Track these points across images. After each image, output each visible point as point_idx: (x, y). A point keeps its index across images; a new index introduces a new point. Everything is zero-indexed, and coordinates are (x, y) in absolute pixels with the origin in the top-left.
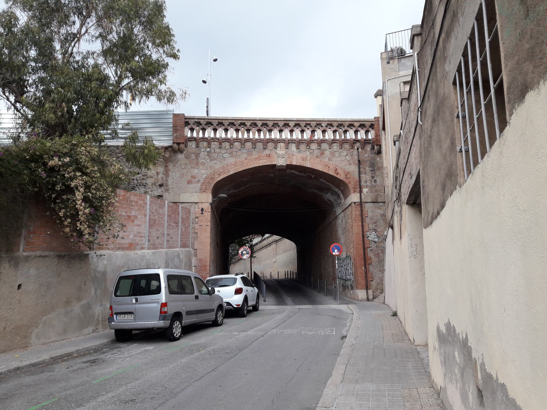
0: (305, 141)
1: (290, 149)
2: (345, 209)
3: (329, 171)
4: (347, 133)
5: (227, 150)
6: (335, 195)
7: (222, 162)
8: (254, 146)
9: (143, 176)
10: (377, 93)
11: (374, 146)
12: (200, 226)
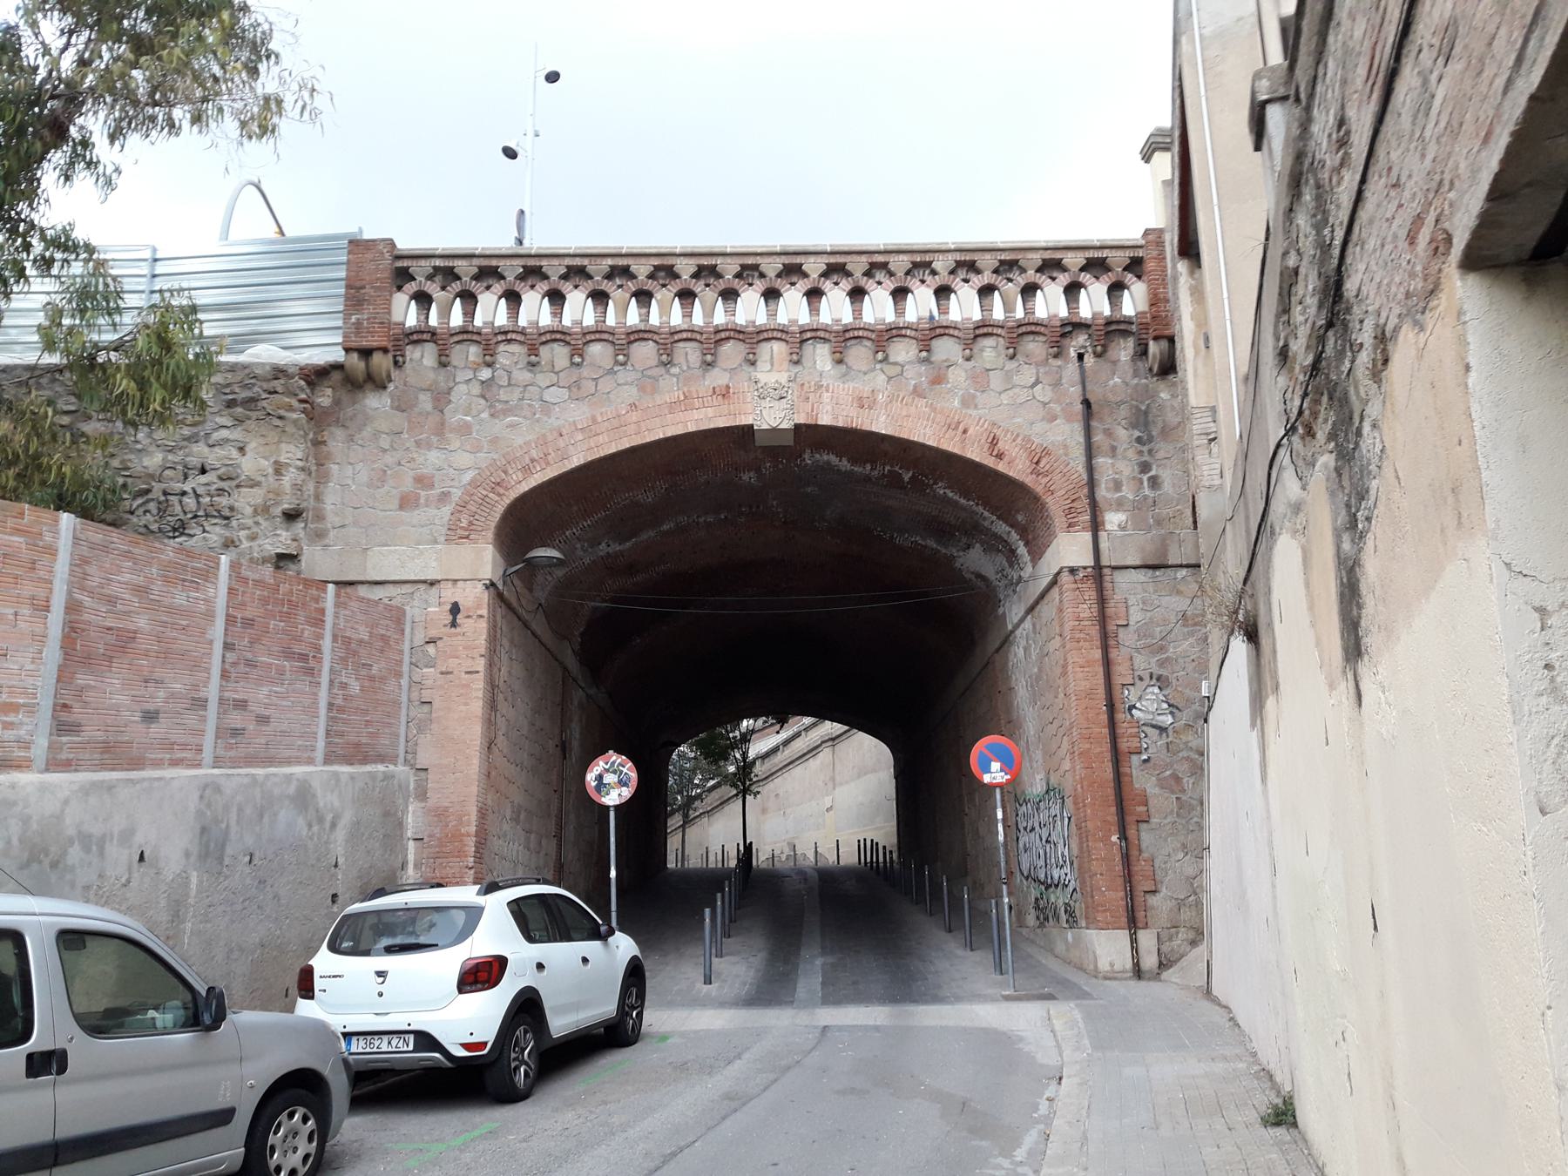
0: (866, 334)
1: (806, 361)
2: (1037, 602)
5: (557, 373)
6: (1000, 551)
9: (221, 478)
11: (1147, 345)
12: (442, 673)
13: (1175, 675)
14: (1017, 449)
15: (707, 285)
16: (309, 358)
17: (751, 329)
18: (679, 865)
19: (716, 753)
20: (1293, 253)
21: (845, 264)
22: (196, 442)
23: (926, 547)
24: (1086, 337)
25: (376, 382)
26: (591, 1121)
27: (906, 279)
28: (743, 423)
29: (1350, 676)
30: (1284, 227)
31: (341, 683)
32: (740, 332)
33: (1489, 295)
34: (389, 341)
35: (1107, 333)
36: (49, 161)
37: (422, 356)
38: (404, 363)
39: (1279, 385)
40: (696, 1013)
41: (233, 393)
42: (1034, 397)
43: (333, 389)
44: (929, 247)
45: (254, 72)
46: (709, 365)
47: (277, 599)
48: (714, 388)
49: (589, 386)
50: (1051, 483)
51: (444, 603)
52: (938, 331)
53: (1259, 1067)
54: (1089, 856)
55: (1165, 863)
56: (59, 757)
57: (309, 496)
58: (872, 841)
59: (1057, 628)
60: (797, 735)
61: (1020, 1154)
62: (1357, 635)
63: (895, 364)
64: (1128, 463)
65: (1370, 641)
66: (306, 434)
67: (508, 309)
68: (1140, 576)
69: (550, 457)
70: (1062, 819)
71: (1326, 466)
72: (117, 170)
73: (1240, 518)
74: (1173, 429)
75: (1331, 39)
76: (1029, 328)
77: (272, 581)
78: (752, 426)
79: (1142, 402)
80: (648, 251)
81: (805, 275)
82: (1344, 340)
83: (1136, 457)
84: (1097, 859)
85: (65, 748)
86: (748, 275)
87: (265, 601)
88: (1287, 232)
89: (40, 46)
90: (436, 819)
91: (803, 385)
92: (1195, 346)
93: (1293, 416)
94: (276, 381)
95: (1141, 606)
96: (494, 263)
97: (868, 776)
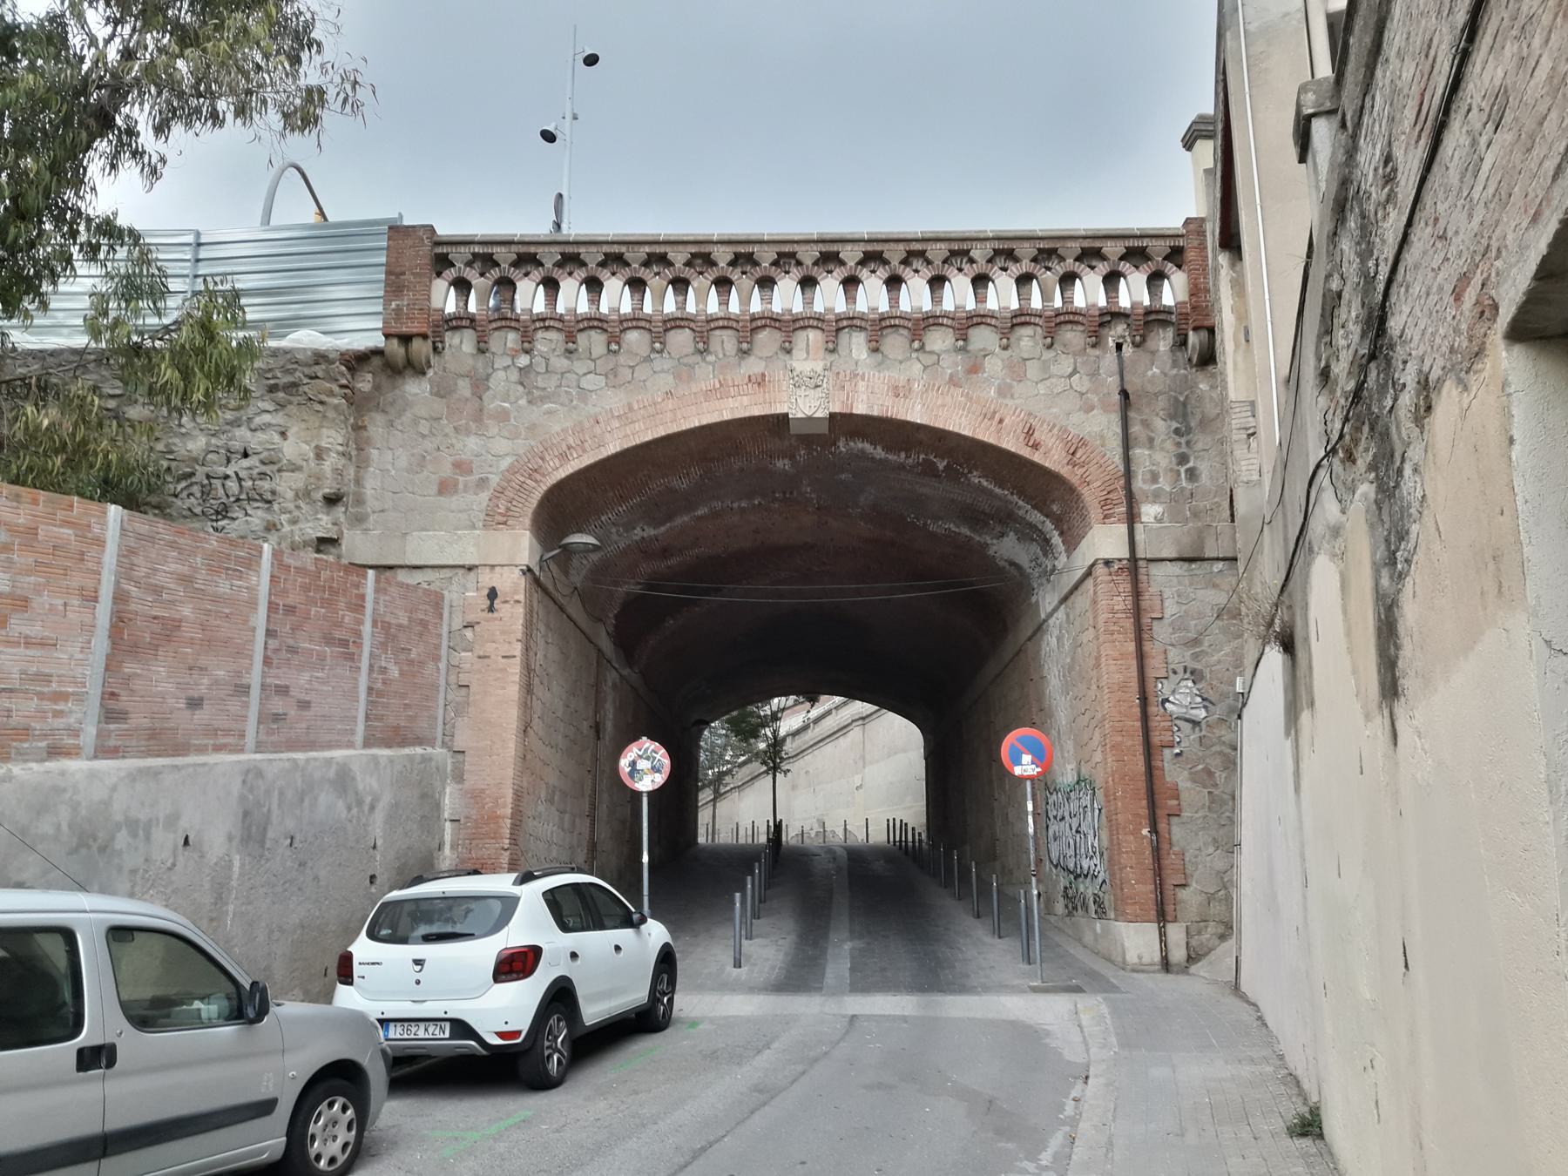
0: (902, 322)
2: (1071, 592)
3: (999, 438)
4: (1073, 284)
6: (1035, 540)
7: (575, 408)
8: (701, 346)
9: (263, 463)
10: (1194, 128)
11: (1186, 335)
12: (480, 657)
16: (348, 344)
17: (787, 317)
18: (710, 841)
19: (746, 731)
20: (1336, 276)
21: (883, 252)
22: (239, 426)
23: (959, 534)
24: (1125, 326)
26: (622, 1111)
27: (943, 267)
28: (778, 411)
29: (1386, 712)
30: (1327, 251)
31: (381, 667)
32: (776, 320)
33: (1534, 367)
34: (429, 327)
35: (1146, 323)
36: (96, 150)
37: (461, 342)
38: (443, 349)
39: (1319, 406)
40: (726, 998)
41: (275, 377)
42: (1071, 387)
43: (373, 374)
44: (967, 235)
45: (295, 60)
46: (745, 353)
47: (319, 586)
48: (749, 377)
49: (626, 374)
52: (975, 320)
53: (1286, 1071)
54: (1120, 849)
55: (1196, 857)
56: (106, 744)
57: (350, 481)
58: (901, 821)
59: (1091, 619)
60: (828, 713)
61: (1046, 1158)
62: (1394, 675)
63: (932, 352)
64: (1165, 454)
65: (1408, 683)
66: (347, 419)
68: (1176, 569)
69: (586, 445)
70: (1093, 810)
71: (1366, 496)
72: (163, 160)
73: (1279, 522)
75: (1379, 73)
77: (314, 568)
78: (787, 414)
79: (1181, 393)
80: (685, 238)
81: (842, 263)
82: (1387, 375)
84: (1127, 852)
85: (113, 734)
86: (784, 263)
87: (306, 588)
88: (1331, 255)
89: (85, 37)
90: (473, 801)
91: (838, 373)
93: (1335, 436)
94: (317, 367)
96: (532, 249)
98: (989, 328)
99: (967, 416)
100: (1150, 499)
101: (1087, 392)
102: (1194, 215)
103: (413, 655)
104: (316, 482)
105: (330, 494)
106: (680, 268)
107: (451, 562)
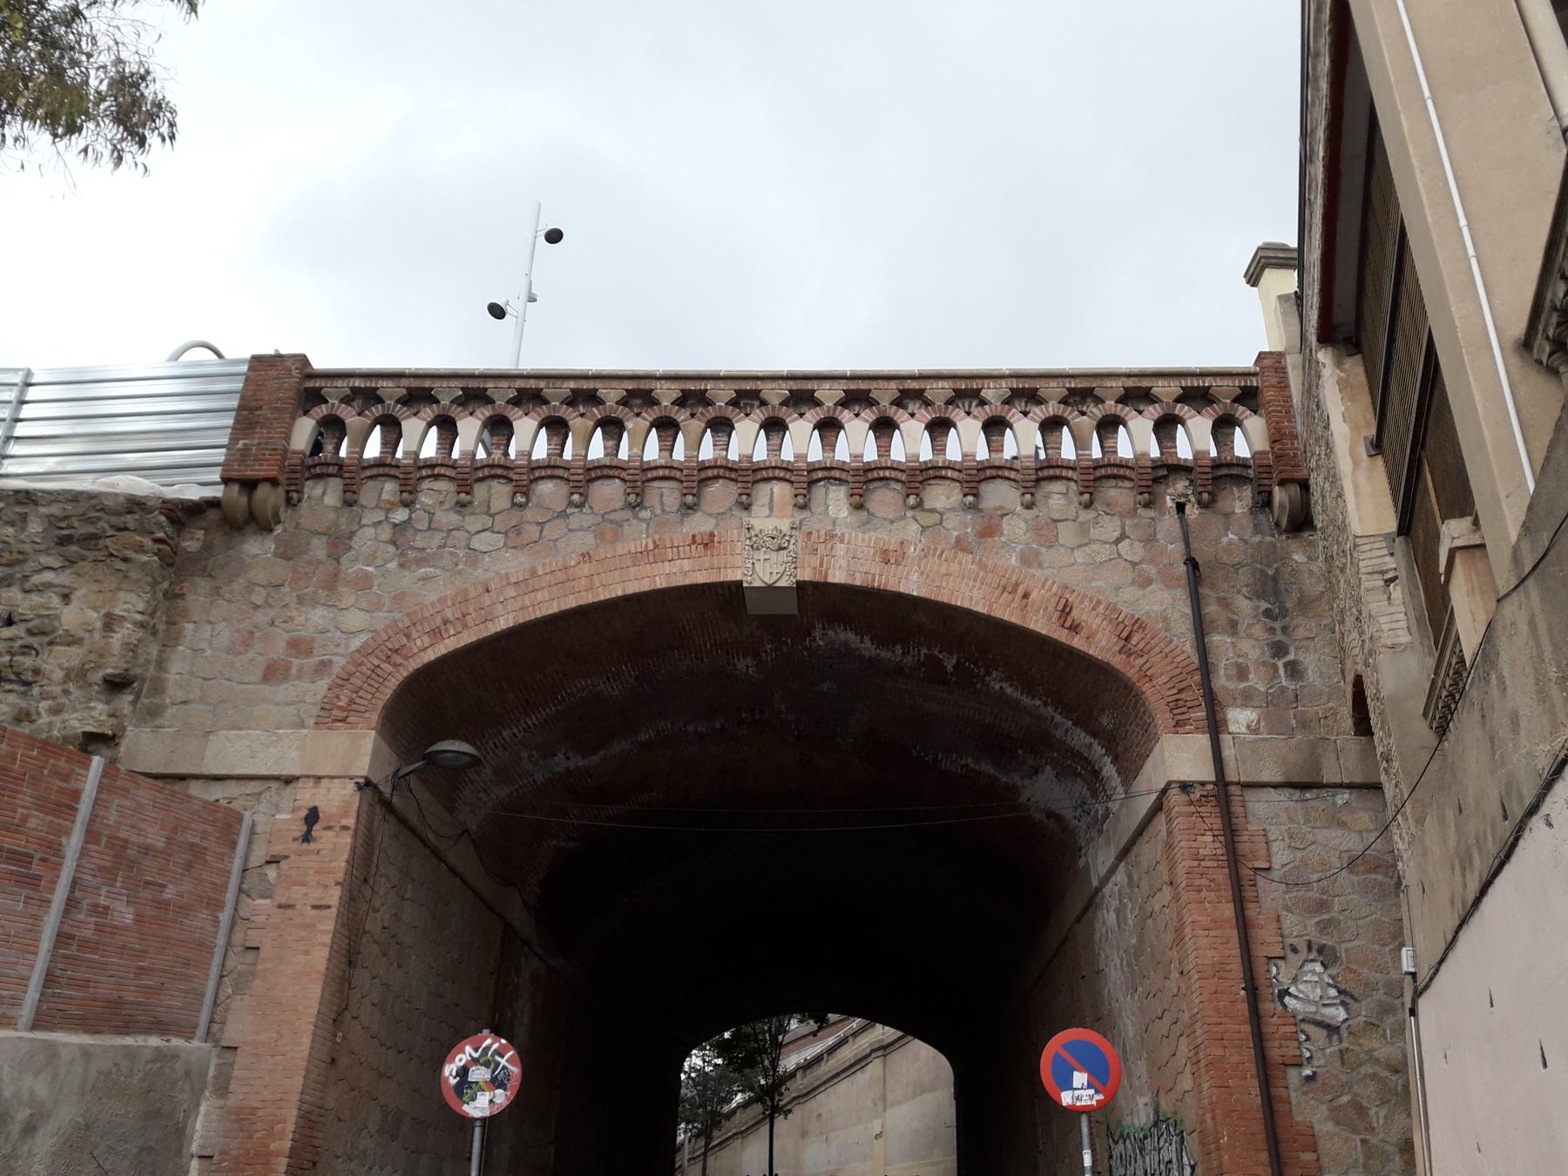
0: (893, 474)
1: (817, 505)
2: (1133, 841)
3: (1024, 617)
4: (1116, 432)
5: (492, 516)
6: (1078, 775)
7: (460, 573)
8: (632, 498)
9: (30, 632)
10: (1260, 254)
11: (1270, 493)
12: (280, 906)
13: (1344, 945)
14: (1098, 621)
15: (693, 415)
21: (869, 391)
22: (9, 585)
24: (1187, 483)
25: (259, 523)
27: (947, 408)
32: (731, 469)
37: (324, 494)
38: (300, 501)
42: (1119, 555)
43: (206, 530)
48: (694, 536)
49: (532, 532)
50: (1148, 665)
51: (299, 808)
57: (148, 661)
67: (439, 439)
69: (469, 618)
70: (1181, 1168)
74: (1314, 601)
76: (1109, 471)
78: (741, 582)
79: (1269, 566)
81: (817, 403)
83: (1266, 635)
91: (810, 534)
92: (1353, 455)
94: (128, 516)
95: (1288, 841)
97: (925, 1095)
98: (1007, 482)
99: (980, 589)
100: (1239, 701)
101: (1140, 562)
102: (1267, 350)
103: (169, 893)
104: (97, 659)
105: (114, 675)
106: (611, 407)
107: (263, 772)
